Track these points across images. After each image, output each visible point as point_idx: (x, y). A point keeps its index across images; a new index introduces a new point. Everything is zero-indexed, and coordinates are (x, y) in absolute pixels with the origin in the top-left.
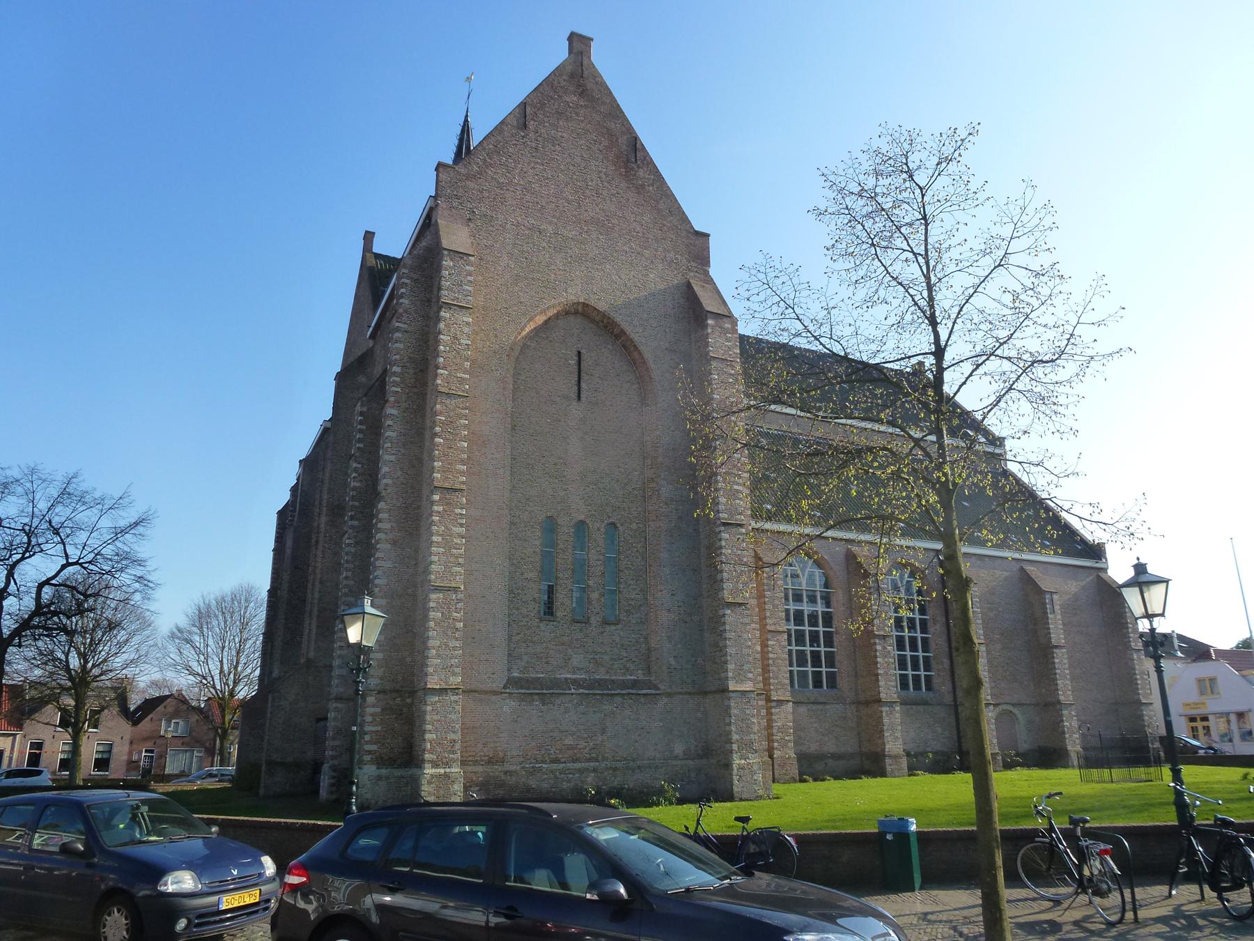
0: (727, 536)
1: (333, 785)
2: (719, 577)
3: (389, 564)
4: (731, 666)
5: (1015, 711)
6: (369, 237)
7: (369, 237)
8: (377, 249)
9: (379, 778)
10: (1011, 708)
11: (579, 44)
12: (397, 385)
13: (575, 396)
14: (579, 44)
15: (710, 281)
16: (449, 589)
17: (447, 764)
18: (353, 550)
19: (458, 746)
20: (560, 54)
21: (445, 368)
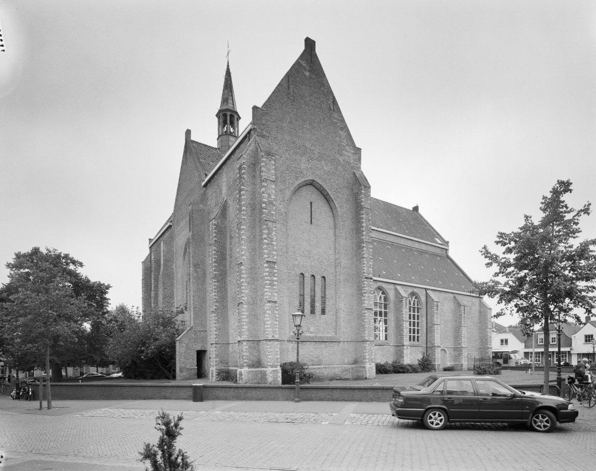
0: (366, 283)
1: (217, 375)
2: (363, 298)
3: (247, 291)
4: (366, 332)
5: (446, 349)
6: (188, 133)
7: (188, 133)
8: (193, 138)
9: (249, 372)
10: (444, 348)
11: (310, 44)
12: (245, 215)
13: (309, 221)
14: (310, 44)
15: (238, 124)
16: (273, 302)
17: (276, 367)
18: (216, 284)
19: (279, 360)
20: (302, 48)
21: (266, 209)
